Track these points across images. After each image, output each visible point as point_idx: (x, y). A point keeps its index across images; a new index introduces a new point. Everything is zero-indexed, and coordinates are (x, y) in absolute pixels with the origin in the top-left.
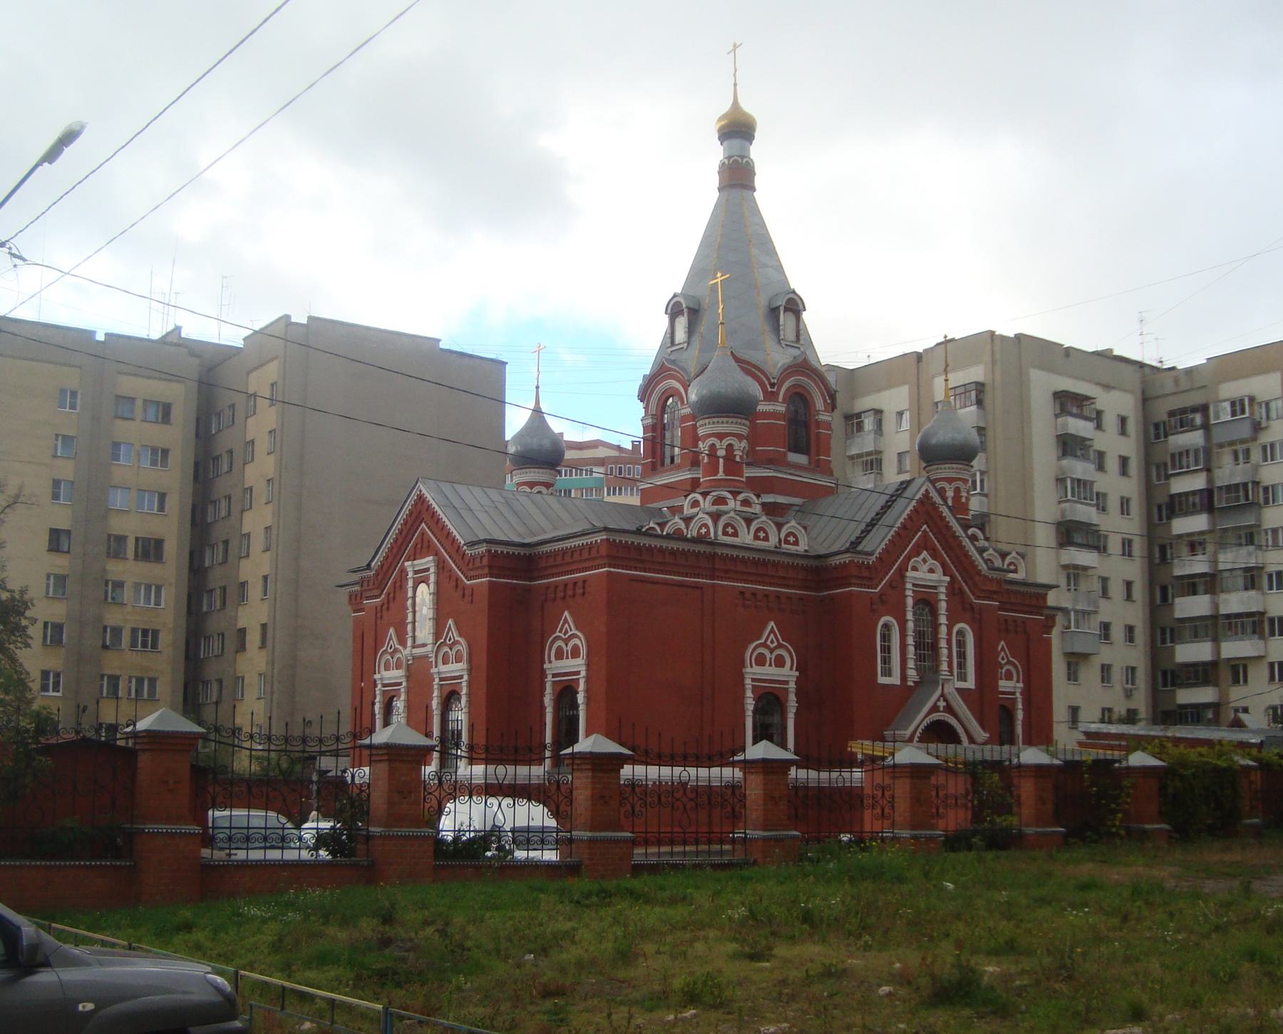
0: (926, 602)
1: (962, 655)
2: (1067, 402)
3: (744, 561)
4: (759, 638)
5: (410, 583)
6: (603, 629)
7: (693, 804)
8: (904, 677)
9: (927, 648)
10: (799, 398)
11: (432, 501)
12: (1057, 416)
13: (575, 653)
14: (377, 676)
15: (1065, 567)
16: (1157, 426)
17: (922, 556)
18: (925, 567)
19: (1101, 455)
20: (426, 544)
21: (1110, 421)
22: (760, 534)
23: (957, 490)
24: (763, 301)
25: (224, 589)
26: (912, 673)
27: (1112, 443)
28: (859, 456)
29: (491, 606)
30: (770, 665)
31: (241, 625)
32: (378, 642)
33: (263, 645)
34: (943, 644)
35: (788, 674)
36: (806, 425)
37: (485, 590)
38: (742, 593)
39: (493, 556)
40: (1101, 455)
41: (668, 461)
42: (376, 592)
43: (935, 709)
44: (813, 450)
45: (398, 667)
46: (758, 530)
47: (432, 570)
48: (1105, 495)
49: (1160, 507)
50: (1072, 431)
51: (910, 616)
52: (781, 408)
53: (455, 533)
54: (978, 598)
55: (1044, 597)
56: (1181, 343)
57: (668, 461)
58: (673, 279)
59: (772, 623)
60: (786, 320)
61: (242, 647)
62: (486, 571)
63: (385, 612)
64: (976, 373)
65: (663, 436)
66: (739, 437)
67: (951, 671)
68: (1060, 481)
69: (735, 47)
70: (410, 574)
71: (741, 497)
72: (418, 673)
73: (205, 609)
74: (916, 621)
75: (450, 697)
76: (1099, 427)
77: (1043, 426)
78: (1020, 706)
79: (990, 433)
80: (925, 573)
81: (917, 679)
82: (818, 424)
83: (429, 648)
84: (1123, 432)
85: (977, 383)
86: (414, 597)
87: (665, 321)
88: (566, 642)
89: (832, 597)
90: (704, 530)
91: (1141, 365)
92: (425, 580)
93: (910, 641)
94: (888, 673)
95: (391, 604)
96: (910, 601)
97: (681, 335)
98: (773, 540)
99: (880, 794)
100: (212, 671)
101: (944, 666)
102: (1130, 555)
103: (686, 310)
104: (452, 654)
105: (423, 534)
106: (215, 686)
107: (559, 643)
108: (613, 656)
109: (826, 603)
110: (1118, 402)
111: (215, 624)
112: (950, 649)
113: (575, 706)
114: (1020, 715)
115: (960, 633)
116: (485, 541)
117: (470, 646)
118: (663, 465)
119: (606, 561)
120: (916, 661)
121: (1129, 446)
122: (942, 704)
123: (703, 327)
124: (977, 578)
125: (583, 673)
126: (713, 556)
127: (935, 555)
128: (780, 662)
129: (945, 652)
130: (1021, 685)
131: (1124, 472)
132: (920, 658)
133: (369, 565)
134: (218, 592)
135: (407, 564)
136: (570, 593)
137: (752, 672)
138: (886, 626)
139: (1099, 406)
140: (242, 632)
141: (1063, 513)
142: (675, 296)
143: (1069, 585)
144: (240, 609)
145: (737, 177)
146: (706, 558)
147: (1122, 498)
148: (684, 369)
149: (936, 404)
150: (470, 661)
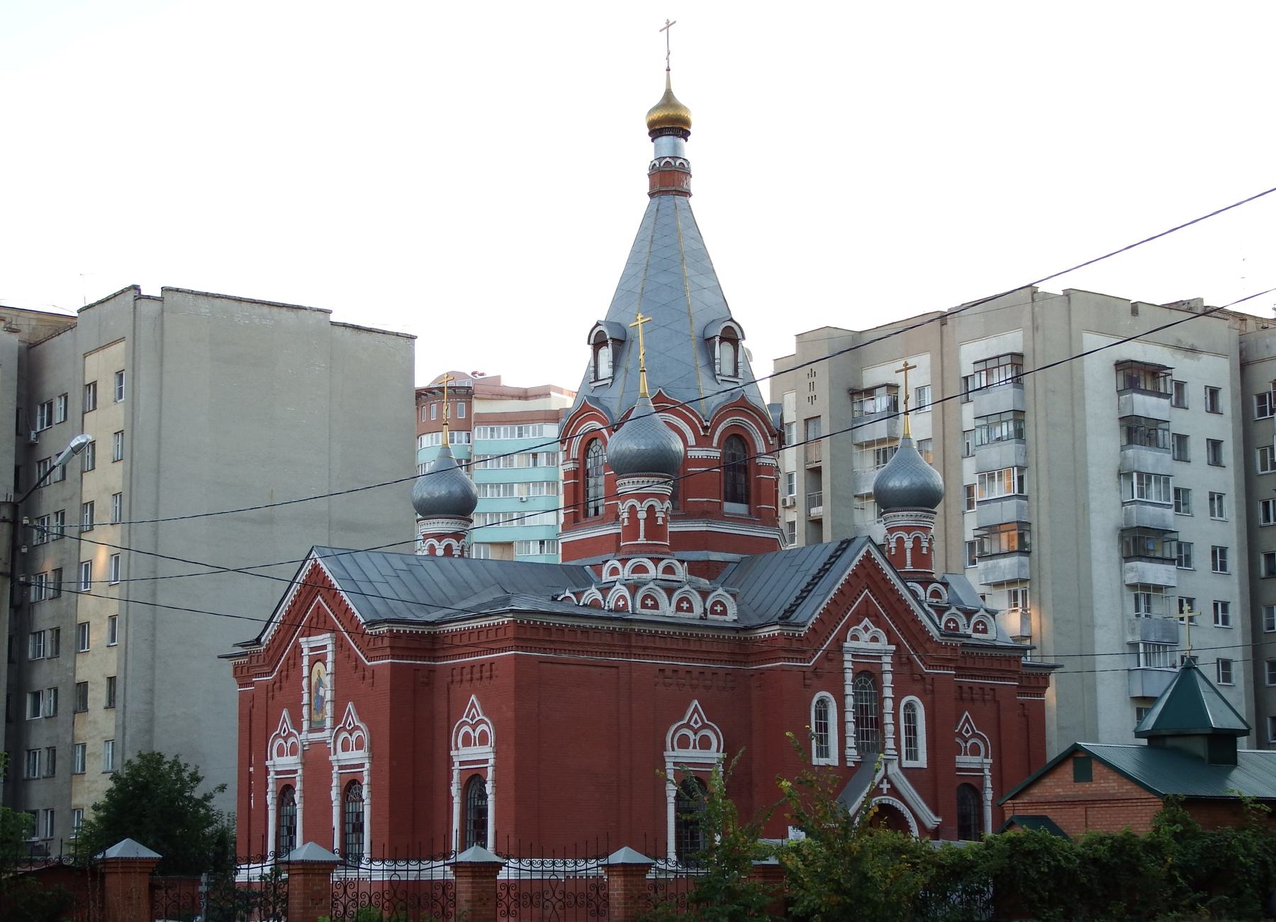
0: (868, 674)
1: (912, 731)
2: (1136, 376)
3: (664, 637)
4: (682, 718)
5: (306, 661)
6: (511, 714)
7: (547, 897)
8: (842, 757)
9: (870, 724)
10: (737, 439)
11: (328, 573)
12: (1119, 392)
13: (483, 739)
14: (268, 763)
15: (1132, 587)
16: (1262, 398)
17: (864, 623)
18: (867, 636)
19: (1181, 440)
20: (322, 619)
21: (1196, 396)
22: (684, 604)
23: (917, 541)
24: (697, 329)
25: (57, 631)
26: (852, 754)
27: (1197, 424)
28: (870, 444)
29: (393, 689)
30: (695, 747)
31: (80, 678)
32: (270, 725)
33: (111, 703)
34: (888, 719)
35: (714, 755)
36: (746, 469)
37: (387, 673)
38: (662, 671)
39: (394, 636)
40: (1181, 440)
41: (592, 511)
42: (266, 669)
43: (877, 791)
44: (752, 500)
45: (293, 752)
46: (681, 600)
47: (330, 648)
48: (1187, 491)
49: (1266, 504)
50: (1139, 412)
51: (849, 690)
52: (716, 454)
53: (354, 610)
54: (930, 667)
55: (1018, 659)
56: (1261, 309)
57: (592, 511)
58: (597, 306)
59: (696, 702)
60: (723, 353)
61: (82, 703)
62: (388, 651)
63: (277, 693)
64: (1012, 341)
65: (586, 483)
66: (661, 497)
67: (898, 749)
68: (1124, 474)
69: (669, 25)
70: (306, 651)
71: (662, 565)
72: (316, 761)
73: (30, 655)
74: (856, 695)
75: (351, 786)
76: (1180, 403)
77: (1101, 401)
78: (989, 784)
79: (1029, 418)
80: (867, 640)
81: (858, 759)
82: (759, 469)
83: (327, 733)
84: (1214, 408)
85: (1012, 354)
86: (310, 677)
87: (589, 350)
88: (474, 727)
89: (762, 672)
90: (621, 603)
91: (1242, 318)
92: (322, 659)
93: (850, 717)
94: (823, 752)
95: (284, 684)
96: (849, 676)
97: (605, 370)
98: (698, 610)
99: (594, 892)
100: (40, 738)
101: (890, 744)
102: (1223, 567)
103: (610, 339)
104: (353, 739)
105: (319, 607)
106: (45, 754)
107: (467, 728)
108: (524, 745)
109: (749, 678)
110: (1207, 370)
111: (44, 676)
112: (897, 725)
113: (484, 796)
114: (989, 795)
115: (909, 706)
116: (386, 621)
117: (370, 731)
118: (586, 515)
119: (513, 643)
120: (857, 739)
121: (1224, 427)
122: (885, 786)
123: (627, 362)
124: (928, 646)
125: (491, 762)
126: (625, 635)
127: (878, 622)
128: (705, 744)
129: (890, 729)
130: (990, 761)
131: (1216, 461)
132: (860, 735)
133: (258, 639)
134: (48, 634)
135: (301, 640)
136: (477, 675)
137: (674, 755)
138: (822, 702)
139: (1177, 376)
140: (82, 688)
141: (1128, 515)
142: (598, 324)
143: (1137, 609)
144: (79, 657)
145: (669, 181)
146: (624, 634)
147: (1212, 495)
148: (607, 410)
149: (966, 378)
150: (371, 749)
